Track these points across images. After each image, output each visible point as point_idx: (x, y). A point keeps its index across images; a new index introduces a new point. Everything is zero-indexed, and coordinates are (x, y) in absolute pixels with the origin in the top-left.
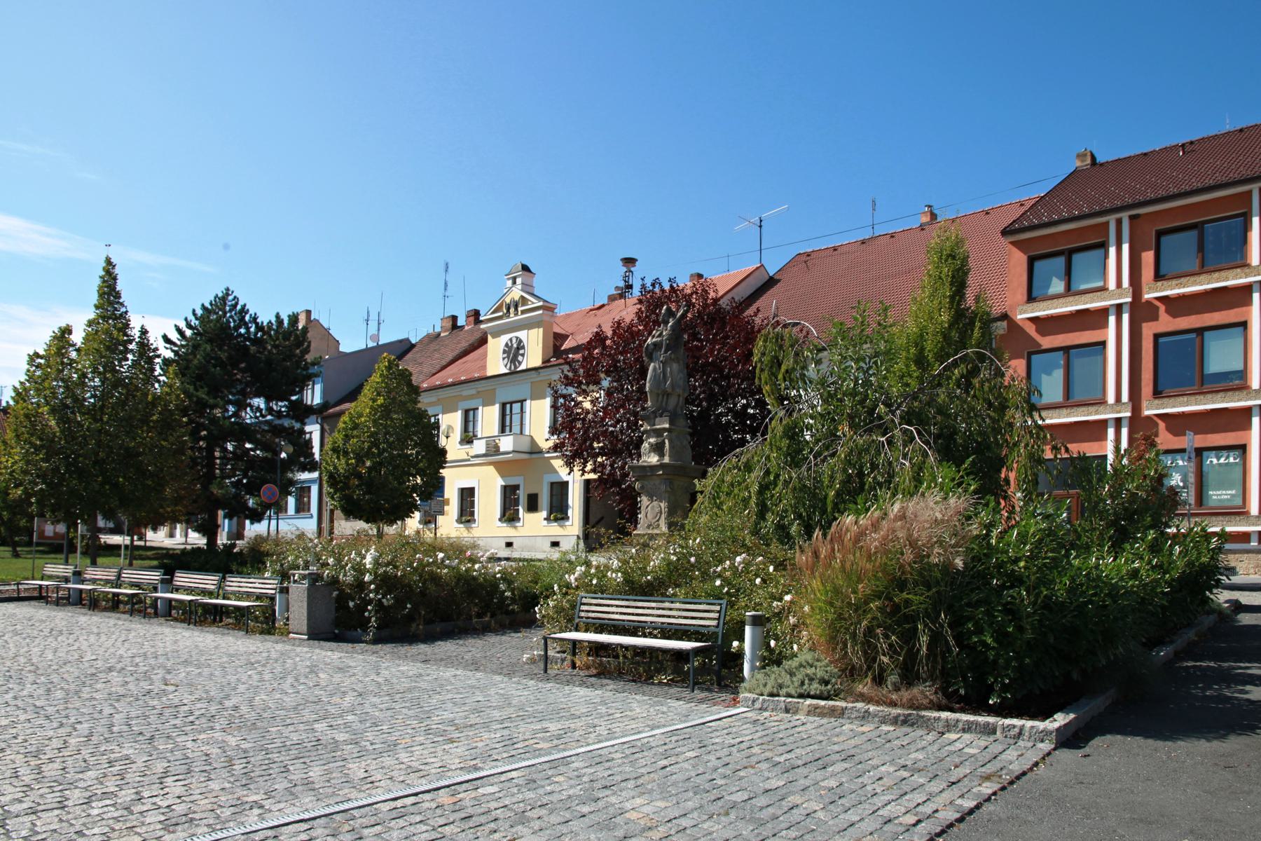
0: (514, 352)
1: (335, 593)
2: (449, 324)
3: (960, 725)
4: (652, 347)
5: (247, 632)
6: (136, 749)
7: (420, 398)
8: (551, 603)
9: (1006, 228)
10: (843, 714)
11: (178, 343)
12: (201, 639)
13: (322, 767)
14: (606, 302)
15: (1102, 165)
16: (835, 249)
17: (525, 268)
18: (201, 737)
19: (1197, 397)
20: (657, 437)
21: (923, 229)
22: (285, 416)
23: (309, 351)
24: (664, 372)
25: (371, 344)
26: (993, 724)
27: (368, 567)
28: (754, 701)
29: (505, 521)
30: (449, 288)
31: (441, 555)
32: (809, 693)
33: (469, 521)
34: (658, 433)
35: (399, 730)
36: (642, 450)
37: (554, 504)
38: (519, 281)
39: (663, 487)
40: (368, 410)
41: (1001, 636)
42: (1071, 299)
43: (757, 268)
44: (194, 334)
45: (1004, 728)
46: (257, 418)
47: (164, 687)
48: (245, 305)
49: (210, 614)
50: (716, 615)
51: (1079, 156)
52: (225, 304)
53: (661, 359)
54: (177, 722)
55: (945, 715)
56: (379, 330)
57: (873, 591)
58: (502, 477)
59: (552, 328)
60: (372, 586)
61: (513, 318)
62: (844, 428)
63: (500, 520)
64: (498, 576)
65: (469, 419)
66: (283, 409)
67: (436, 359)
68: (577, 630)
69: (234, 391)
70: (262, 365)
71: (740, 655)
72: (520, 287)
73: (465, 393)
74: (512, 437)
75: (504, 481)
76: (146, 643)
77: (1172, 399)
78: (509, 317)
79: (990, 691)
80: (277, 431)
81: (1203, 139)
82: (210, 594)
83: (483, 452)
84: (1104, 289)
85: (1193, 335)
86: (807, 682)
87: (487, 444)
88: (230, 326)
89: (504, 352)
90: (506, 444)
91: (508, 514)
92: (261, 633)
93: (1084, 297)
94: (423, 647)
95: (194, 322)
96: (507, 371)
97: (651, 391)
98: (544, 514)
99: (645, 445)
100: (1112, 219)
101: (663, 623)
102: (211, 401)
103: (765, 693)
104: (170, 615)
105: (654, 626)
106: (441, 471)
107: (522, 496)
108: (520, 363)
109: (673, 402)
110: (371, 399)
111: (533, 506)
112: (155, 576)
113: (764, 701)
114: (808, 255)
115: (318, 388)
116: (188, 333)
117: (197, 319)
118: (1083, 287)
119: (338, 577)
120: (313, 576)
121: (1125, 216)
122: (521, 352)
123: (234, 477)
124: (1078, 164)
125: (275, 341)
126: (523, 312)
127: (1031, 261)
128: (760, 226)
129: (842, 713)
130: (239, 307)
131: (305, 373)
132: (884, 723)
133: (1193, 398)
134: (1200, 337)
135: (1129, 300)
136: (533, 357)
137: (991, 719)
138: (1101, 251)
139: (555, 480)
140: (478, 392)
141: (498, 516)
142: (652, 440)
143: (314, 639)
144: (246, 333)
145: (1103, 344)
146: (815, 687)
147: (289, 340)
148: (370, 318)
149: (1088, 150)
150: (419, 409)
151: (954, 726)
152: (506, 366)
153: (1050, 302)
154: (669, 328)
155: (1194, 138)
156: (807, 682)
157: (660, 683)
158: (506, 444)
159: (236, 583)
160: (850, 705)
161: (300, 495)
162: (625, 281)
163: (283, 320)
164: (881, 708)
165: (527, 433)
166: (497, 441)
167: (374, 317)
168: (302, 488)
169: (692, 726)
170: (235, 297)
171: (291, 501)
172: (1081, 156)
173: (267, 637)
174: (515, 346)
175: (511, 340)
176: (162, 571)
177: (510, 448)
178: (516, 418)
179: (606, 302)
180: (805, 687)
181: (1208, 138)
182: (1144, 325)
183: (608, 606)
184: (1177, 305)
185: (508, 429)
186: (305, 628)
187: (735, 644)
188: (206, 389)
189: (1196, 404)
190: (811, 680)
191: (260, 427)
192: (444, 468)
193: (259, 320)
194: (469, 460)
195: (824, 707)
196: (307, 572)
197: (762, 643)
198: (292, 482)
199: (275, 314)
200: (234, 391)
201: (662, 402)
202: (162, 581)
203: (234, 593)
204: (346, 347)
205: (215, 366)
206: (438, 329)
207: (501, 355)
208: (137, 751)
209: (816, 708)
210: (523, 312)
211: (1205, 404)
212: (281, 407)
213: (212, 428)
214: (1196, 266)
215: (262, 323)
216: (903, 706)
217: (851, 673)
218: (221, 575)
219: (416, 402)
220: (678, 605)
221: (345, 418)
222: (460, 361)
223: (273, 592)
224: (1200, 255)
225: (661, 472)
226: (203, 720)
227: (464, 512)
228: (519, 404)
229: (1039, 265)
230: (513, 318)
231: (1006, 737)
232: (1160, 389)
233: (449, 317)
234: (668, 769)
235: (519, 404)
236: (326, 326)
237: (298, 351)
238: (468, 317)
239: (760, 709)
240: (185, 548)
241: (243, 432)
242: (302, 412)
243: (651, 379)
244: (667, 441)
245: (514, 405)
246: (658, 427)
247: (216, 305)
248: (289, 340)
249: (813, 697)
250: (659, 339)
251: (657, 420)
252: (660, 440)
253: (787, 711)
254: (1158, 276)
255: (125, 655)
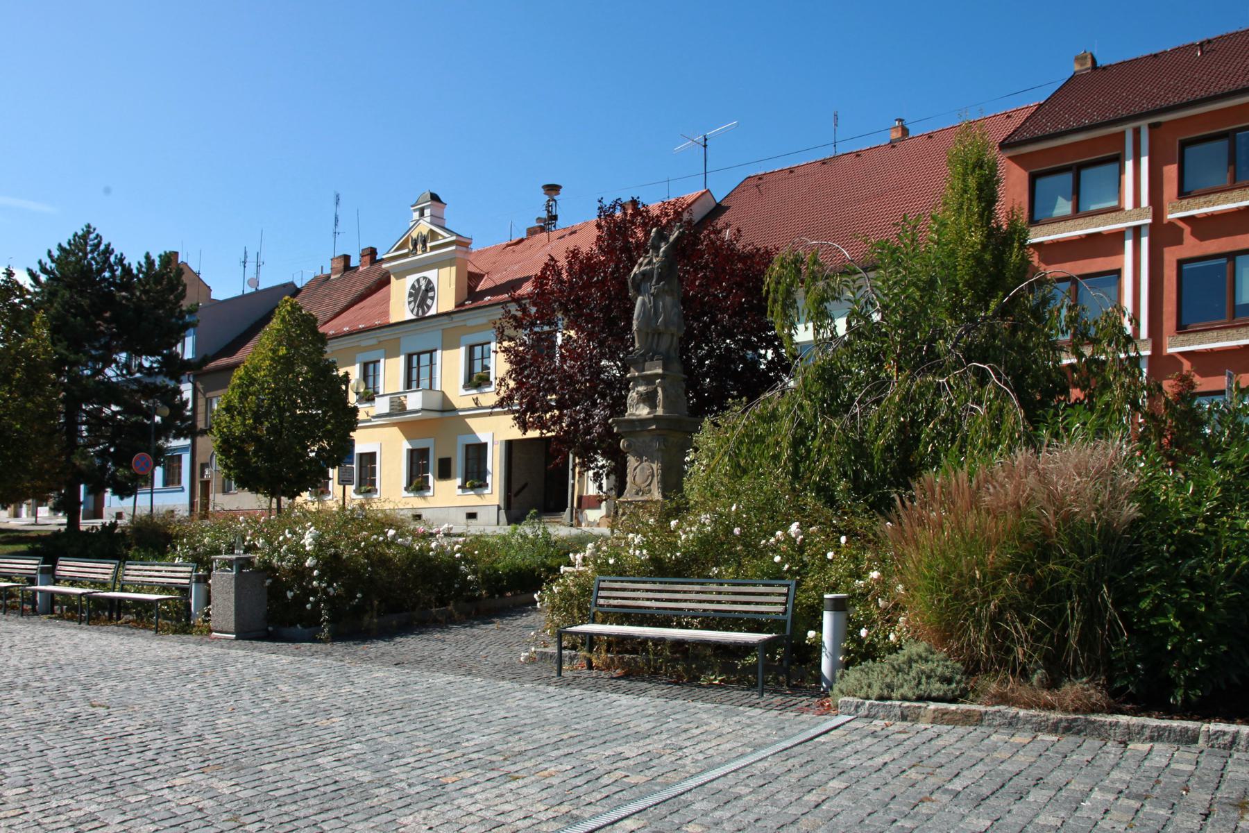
0: (422, 295)
1: (268, 582)
2: (341, 265)
3: (1147, 733)
4: (640, 277)
5: (157, 632)
6: (99, 804)
7: (327, 349)
8: (555, 589)
9: (1005, 140)
10: (982, 720)
11: (32, 290)
12: (105, 643)
13: (365, 824)
14: (524, 235)
15: (1105, 68)
16: (791, 171)
17: (435, 198)
18: (178, 782)
19: (1229, 331)
20: (647, 385)
21: (893, 147)
22: (157, 374)
23: (184, 296)
24: (655, 307)
25: (249, 290)
26: (1194, 731)
27: (308, 548)
28: (857, 707)
29: (413, 490)
30: (340, 223)
31: (391, 532)
32: (929, 695)
33: (369, 491)
34: (649, 380)
35: (432, 764)
36: (629, 401)
37: (470, 470)
38: (427, 212)
39: (656, 445)
40: (267, 363)
41: (1186, 614)
42: (1081, 221)
43: (703, 194)
44: (50, 279)
45: (1209, 736)
46: (123, 376)
47: (91, 710)
48: (109, 245)
49: (104, 609)
50: (783, 599)
51: (1077, 59)
52: (86, 244)
53: (652, 291)
54: (133, 760)
55: (1123, 719)
56: (258, 273)
57: (1004, 563)
58: (408, 439)
59: (466, 266)
60: (316, 573)
61: (420, 256)
62: (890, 369)
63: (406, 489)
64: (458, 555)
65: (369, 372)
66: (155, 365)
67: (329, 305)
68: (594, 621)
69: (97, 344)
70: (130, 313)
71: (817, 647)
72: (428, 219)
73: (363, 344)
74: (420, 393)
75: (411, 444)
76: (40, 649)
77: (1200, 335)
78: (415, 254)
79: (1171, 685)
80: (149, 391)
81: (1178, 48)
82: (103, 585)
83: (387, 410)
84: (1119, 209)
85: (1223, 261)
86: (924, 680)
87: (392, 402)
88: (92, 269)
89: (410, 295)
90: (414, 401)
91: (417, 483)
92: (175, 632)
93: (1096, 219)
94: (382, 646)
95: (50, 265)
96: (414, 317)
97: (639, 330)
98: (459, 481)
99: (633, 395)
100: (1128, 128)
101: (705, 610)
102: (72, 357)
103: (874, 697)
104: (53, 612)
105: (694, 614)
106: (351, 434)
107: (433, 464)
108: (429, 307)
109: (665, 343)
110: (270, 350)
111: (445, 472)
112: (31, 565)
113: (871, 706)
114: (760, 179)
115: (189, 341)
116: (43, 278)
117: (53, 261)
118: (1093, 207)
119: (270, 562)
120: (241, 562)
121: (1144, 125)
122: (431, 294)
123: (98, 445)
124: (1077, 68)
125: (144, 286)
126: (433, 248)
127: (1033, 179)
128: (705, 146)
129: (980, 719)
130: (102, 247)
131: (181, 322)
132: (1039, 731)
133: (1224, 333)
134: (1231, 262)
135: (1149, 221)
136: (445, 300)
137: (1191, 725)
138: (1115, 166)
139: (471, 441)
140: (380, 342)
141: (404, 484)
142: (641, 389)
143: (244, 639)
144: (111, 277)
145: (1118, 273)
146: (937, 688)
147: (161, 284)
148: (248, 260)
149: (1088, 52)
150: (327, 360)
151: (1138, 734)
152: (412, 311)
153: (1055, 225)
154: (661, 254)
155: (1210, 37)
156: (924, 680)
157: (711, 685)
158: (414, 401)
159: (136, 572)
160: (991, 709)
161: (169, 466)
162: (549, 212)
163: (153, 261)
164: (1032, 712)
165: (438, 388)
166: (402, 398)
167: (252, 258)
168: (172, 457)
169: (801, 743)
170: (98, 235)
171: (159, 472)
172: (1080, 59)
173: (185, 637)
174: (423, 287)
175: (418, 280)
176: (41, 558)
177: (419, 406)
178: (425, 371)
179: (525, 236)
180: (923, 687)
181: (1229, 36)
182: (1166, 250)
183: (634, 590)
184: (1204, 227)
185: (414, 384)
186: (232, 626)
187: (811, 634)
188: (66, 343)
189: (1227, 340)
190: (929, 677)
191: (128, 387)
192: (354, 430)
193: (126, 262)
194: (370, 421)
195: (955, 712)
196: (234, 557)
197: (848, 630)
198: (160, 452)
199: (144, 254)
200: (97, 344)
201: (652, 343)
202: (43, 571)
203: (132, 583)
204: (219, 294)
205: (75, 316)
206: (327, 271)
207: (406, 299)
208: (101, 807)
209: (944, 714)
210: (433, 248)
211: (1238, 339)
212: (152, 362)
213: (74, 388)
214: (1226, 180)
215: (130, 264)
216: (1066, 710)
217: (973, 668)
218: (117, 562)
219: (322, 353)
220: (726, 588)
221: (240, 372)
222: (356, 307)
223: (187, 581)
224: (1231, 168)
225: (654, 427)
226: (167, 757)
227: (469, 475)
228: (428, 355)
229: (1041, 184)
230: (420, 256)
231: (1212, 746)
232: (1183, 323)
233: (340, 257)
234: (824, 807)
235: (428, 355)
236: (195, 270)
237: (172, 297)
238: (362, 256)
239: (866, 717)
240: (59, 530)
241: (110, 392)
242: (176, 368)
243: (639, 315)
244: (660, 390)
245: (422, 356)
246: (649, 372)
247: (76, 245)
248: (161, 284)
249: (936, 700)
250: (649, 267)
251: (647, 364)
252: (651, 388)
253: (904, 718)
254: (1183, 193)
255: (22, 666)
